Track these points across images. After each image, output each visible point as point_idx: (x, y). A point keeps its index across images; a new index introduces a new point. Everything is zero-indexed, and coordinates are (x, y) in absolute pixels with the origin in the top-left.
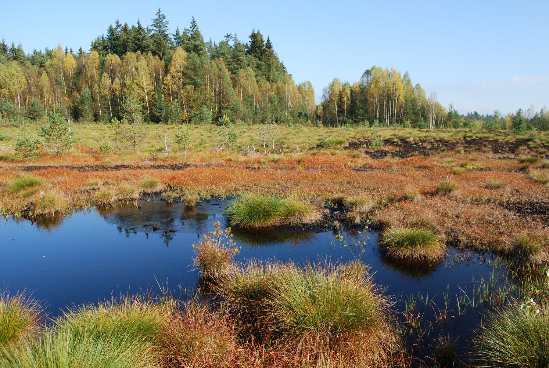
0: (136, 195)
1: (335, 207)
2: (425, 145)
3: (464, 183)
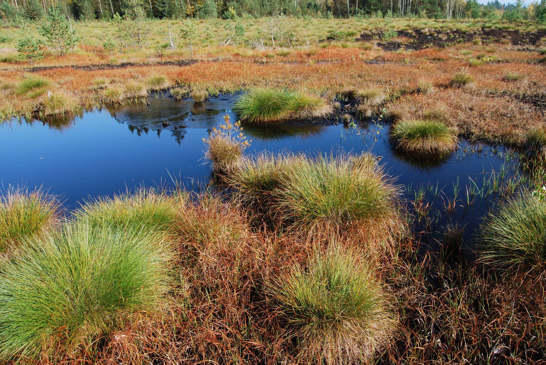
0: (144, 93)
1: (346, 100)
2: (440, 36)
3: (480, 76)
